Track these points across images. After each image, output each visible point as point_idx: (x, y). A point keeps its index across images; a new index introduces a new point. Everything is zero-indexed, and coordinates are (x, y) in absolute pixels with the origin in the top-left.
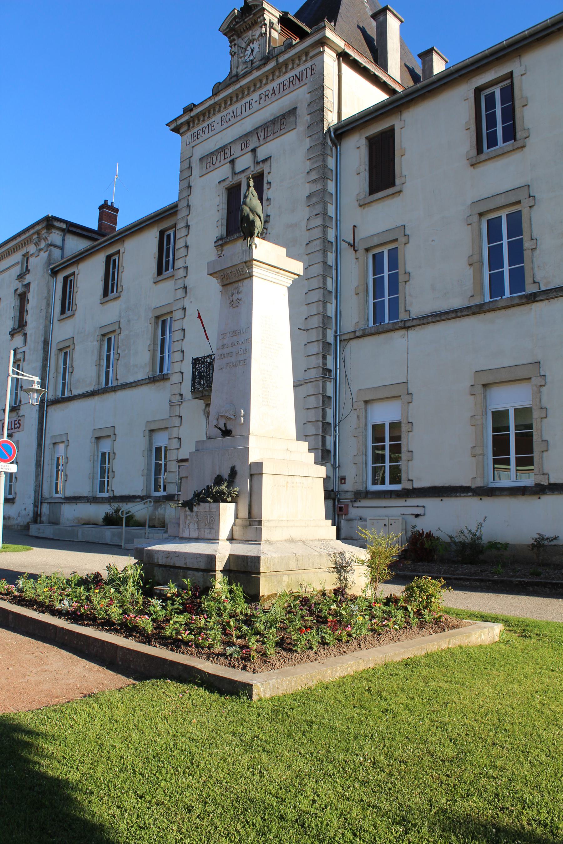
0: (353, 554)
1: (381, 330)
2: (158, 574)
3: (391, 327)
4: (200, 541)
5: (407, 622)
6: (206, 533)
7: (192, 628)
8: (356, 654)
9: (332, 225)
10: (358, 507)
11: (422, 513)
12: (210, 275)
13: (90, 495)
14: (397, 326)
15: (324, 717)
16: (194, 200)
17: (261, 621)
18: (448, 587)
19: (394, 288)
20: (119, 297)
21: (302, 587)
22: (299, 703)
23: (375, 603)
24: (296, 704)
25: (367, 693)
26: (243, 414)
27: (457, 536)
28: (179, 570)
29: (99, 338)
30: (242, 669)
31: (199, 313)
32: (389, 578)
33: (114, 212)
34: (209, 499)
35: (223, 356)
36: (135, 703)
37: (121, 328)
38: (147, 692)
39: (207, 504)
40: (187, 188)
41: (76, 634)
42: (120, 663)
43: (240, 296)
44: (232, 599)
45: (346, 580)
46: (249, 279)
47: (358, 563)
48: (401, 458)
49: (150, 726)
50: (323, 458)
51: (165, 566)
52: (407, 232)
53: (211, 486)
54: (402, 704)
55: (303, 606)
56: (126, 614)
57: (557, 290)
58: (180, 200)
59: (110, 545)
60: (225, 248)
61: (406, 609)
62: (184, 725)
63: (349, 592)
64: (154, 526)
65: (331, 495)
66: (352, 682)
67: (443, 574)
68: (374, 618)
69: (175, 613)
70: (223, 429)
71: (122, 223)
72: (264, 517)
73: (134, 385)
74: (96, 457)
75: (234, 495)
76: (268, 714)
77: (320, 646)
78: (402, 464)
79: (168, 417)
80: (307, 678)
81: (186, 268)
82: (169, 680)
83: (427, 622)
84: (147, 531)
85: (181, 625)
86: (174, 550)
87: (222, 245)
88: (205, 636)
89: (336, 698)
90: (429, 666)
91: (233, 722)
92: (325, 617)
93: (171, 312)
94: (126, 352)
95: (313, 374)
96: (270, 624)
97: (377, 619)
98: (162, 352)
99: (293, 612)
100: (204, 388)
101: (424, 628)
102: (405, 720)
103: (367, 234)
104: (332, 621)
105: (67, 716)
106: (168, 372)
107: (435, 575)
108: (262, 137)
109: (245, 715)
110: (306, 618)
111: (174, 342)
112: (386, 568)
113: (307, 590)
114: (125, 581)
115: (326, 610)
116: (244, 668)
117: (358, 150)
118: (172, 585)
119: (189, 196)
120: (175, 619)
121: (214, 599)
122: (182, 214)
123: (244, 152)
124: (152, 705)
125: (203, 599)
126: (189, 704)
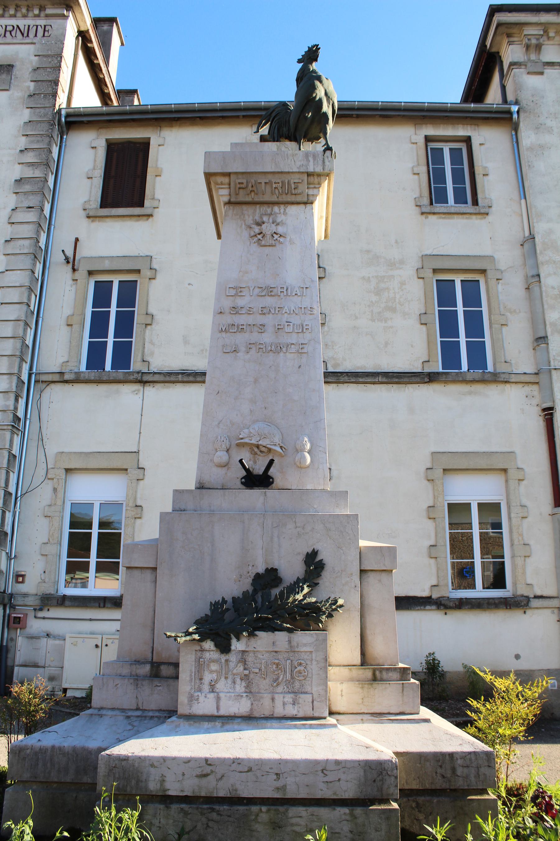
10: (44, 618)
14: (131, 378)
26: (308, 446)
52: (155, 266)
57: (349, 374)
103: (94, 254)
117: (93, 151)
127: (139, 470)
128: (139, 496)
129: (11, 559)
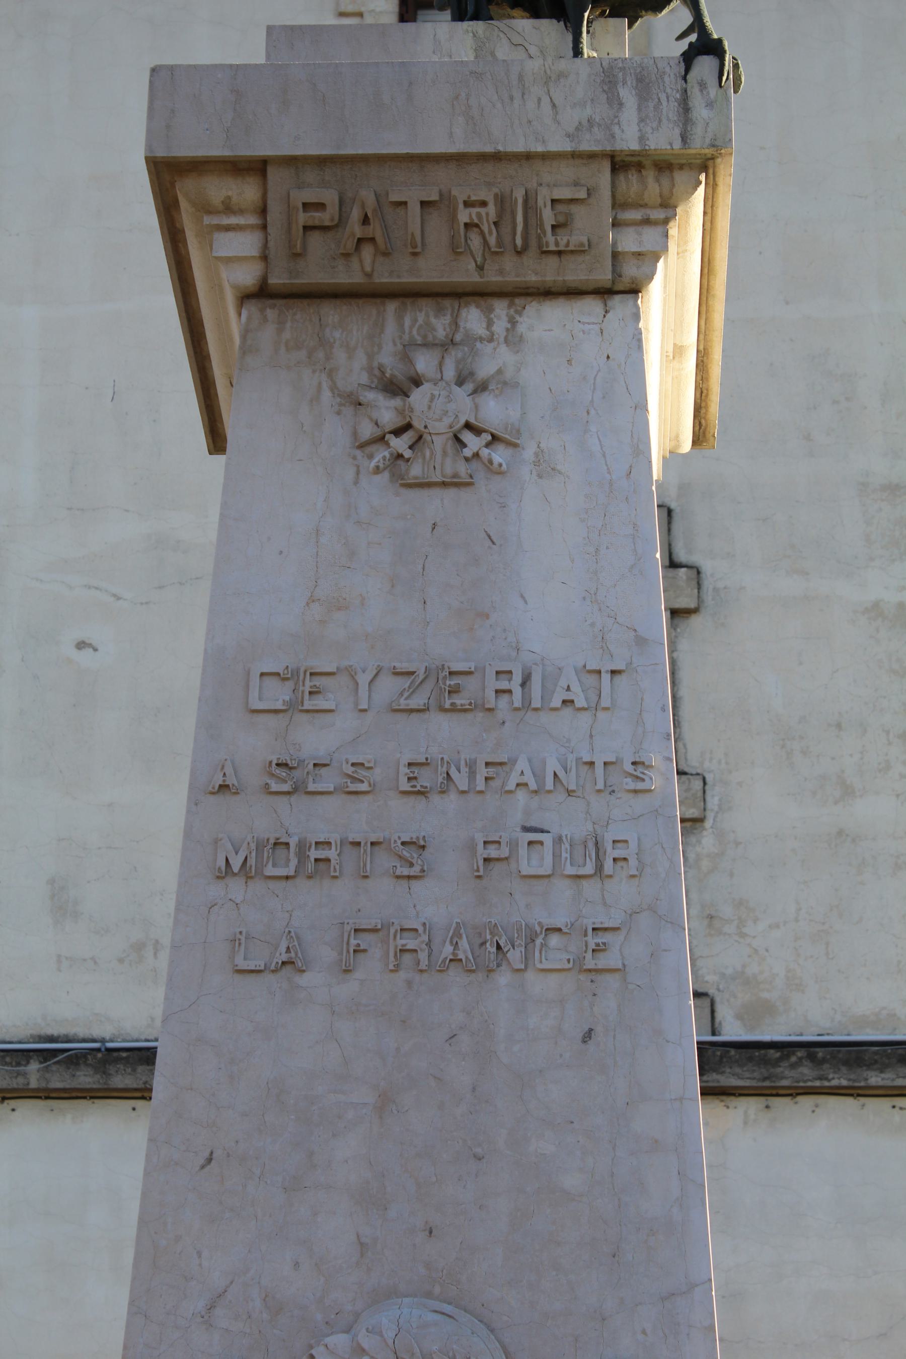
43: (493, 411)
46: (592, 306)
57: (820, 1053)
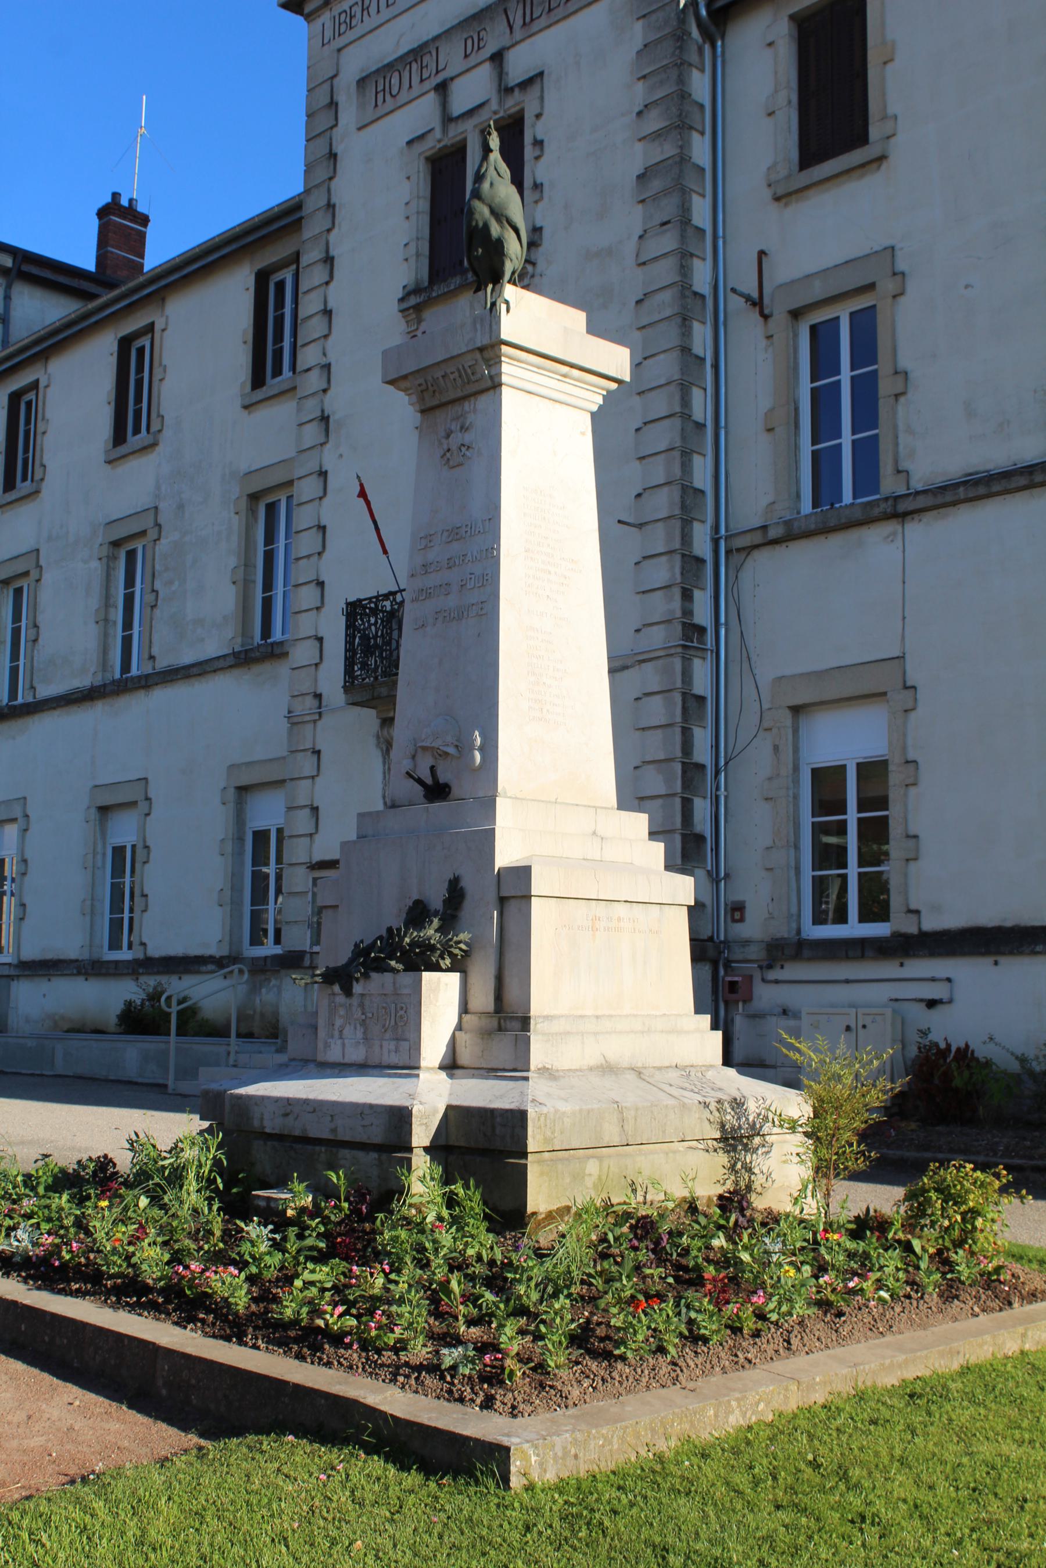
0: (768, 1102)
1: (832, 523)
2: (263, 1156)
3: (858, 514)
4: (371, 1071)
5: (911, 1283)
6: (385, 1050)
7: (351, 1298)
8: (778, 1366)
9: (704, 251)
10: (777, 982)
11: (945, 996)
12: (391, 382)
13: (85, 955)
14: (876, 512)
15: (697, 1534)
16: (346, 189)
17: (530, 1279)
18: (1018, 1192)
19: (866, 412)
20: (154, 445)
21: (634, 1191)
22: (631, 1497)
23: (825, 1231)
24: (625, 1501)
25: (809, 1470)
26: (478, 741)
27: (1037, 1058)
28: (317, 1148)
29: (105, 551)
30: (482, 1407)
31: (362, 485)
32: (861, 1165)
33: (135, 222)
34: (393, 963)
35: (425, 594)
36: (202, 1499)
37: (160, 526)
38: (233, 1469)
39: (388, 976)
40: (323, 159)
41: (48, 1318)
42: (164, 1392)
43: (468, 437)
44: (455, 1220)
45: (750, 1170)
46: (491, 392)
47: (781, 1126)
48: (887, 854)
49: (243, 1559)
50: (685, 856)
51: (280, 1137)
52: (901, 265)
53: (399, 930)
54: (905, 1501)
55: (640, 1239)
56: (180, 1263)
58: (307, 191)
59: (136, 1083)
60: (427, 314)
61: (908, 1247)
62: (331, 1556)
63: (759, 1203)
64: (250, 1035)
65: (707, 951)
66: (771, 1440)
67: (1002, 1157)
68: (826, 1271)
69: (308, 1258)
70: (429, 781)
71: (159, 250)
72: (538, 1006)
73: (195, 671)
74: (99, 857)
75: (456, 951)
76: (551, 1526)
77: (684, 1345)
78: (890, 869)
79: (286, 754)
80: (653, 1431)
81: (327, 367)
82: (291, 1438)
83: (963, 1283)
84: (233, 1048)
85: (323, 1290)
86: (303, 1096)
87: (418, 308)
88: (384, 1320)
89: (728, 1484)
90: (973, 1401)
91: (459, 1549)
92: (698, 1268)
93: (290, 483)
94: (174, 588)
95: (657, 638)
96: (551, 1287)
97: (833, 1274)
98: (268, 584)
99: (613, 1256)
100: (376, 678)
101: (957, 1297)
102: (911, 1544)
103: (796, 273)
104: (714, 1279)
105: (25, 1536)
106: (286, 637)
107: (981, 1159)
108: (519, 22)
109: (490, 1528)
110: (648, 1271)
111: (298, 559)
112: (854, 1140)
113: (649, 1198)
114: (176, 1177)
115: (699, 1250)
116: (488, 1404)
118: (299, 1187)
119: (331, 179)
120: (307, 1276)
121: (408, 1221)
122: (312, 228)
123: (473, 60)
124: (247, 1502)
125: (378, 1222)
126: (343, 1499)
127: (906, 692)
128: (910, 742)
129: (718, 883)
